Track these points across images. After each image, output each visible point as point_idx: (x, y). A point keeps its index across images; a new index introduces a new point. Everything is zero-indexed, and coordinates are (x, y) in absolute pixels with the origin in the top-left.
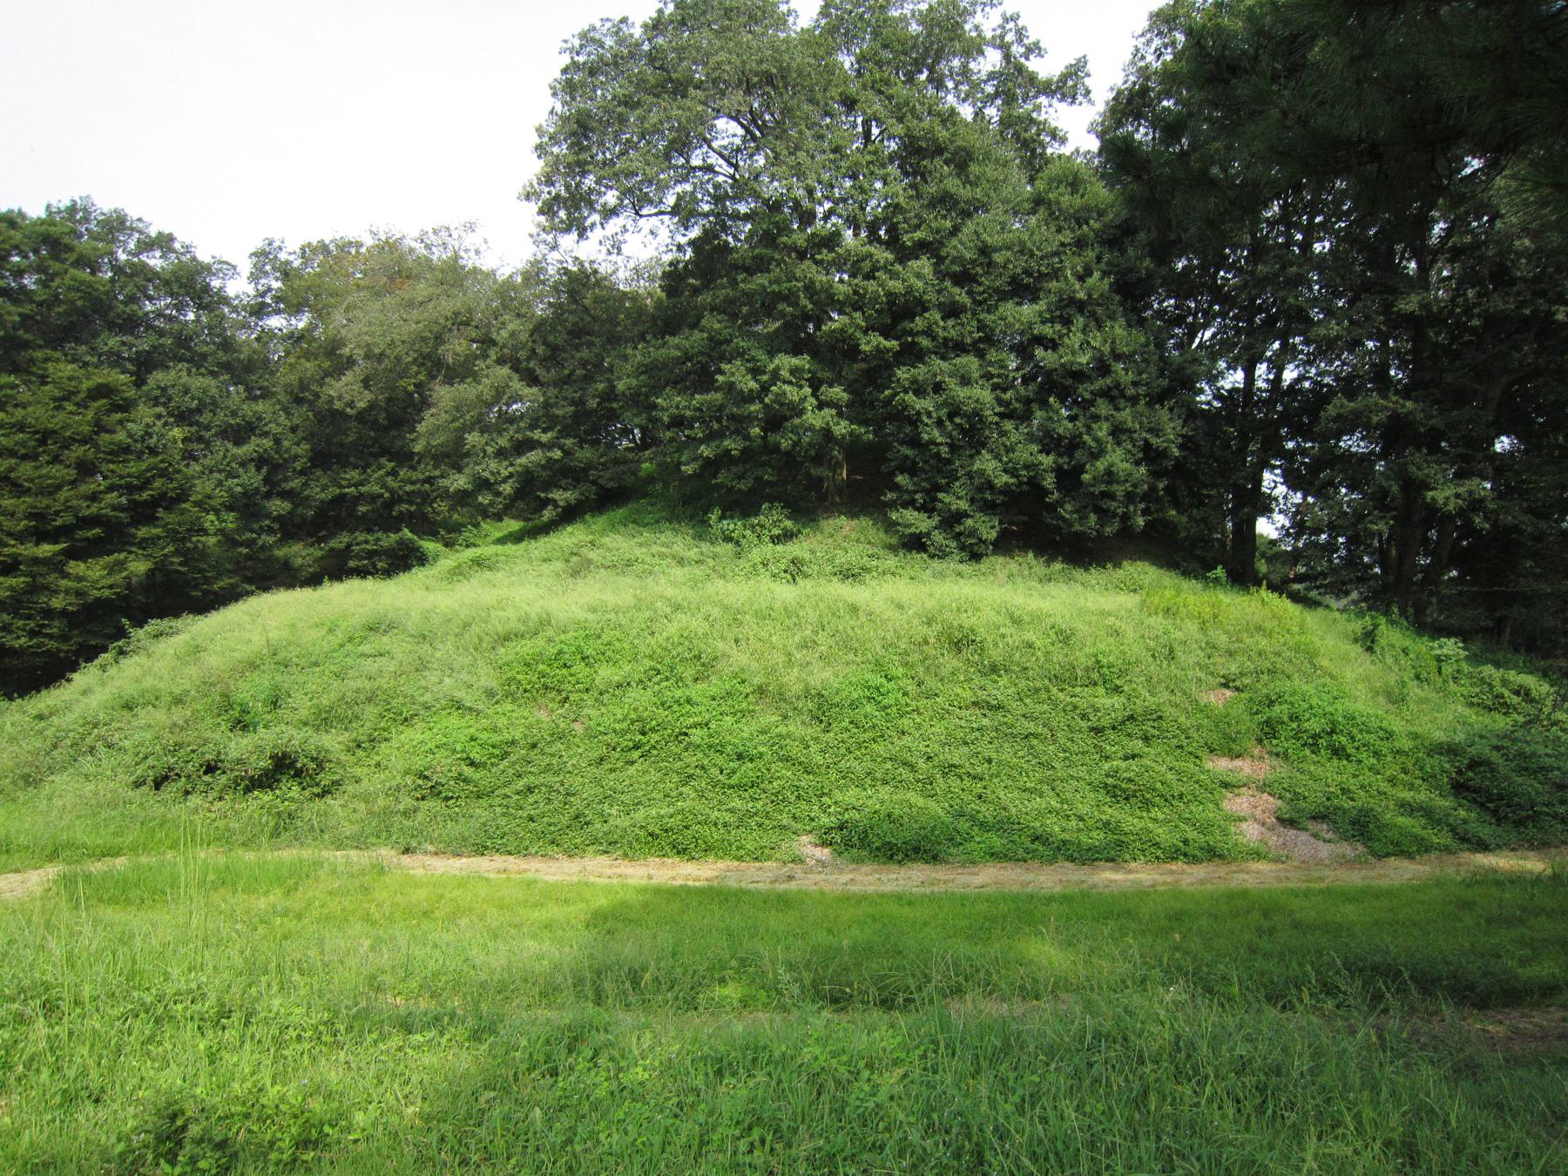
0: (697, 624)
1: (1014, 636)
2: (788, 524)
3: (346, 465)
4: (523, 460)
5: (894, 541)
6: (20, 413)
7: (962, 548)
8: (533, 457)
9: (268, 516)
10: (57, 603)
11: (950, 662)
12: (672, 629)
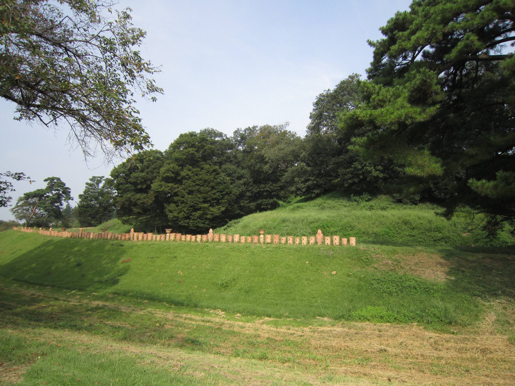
0: (350, 220)
1: (418, 221)
2: (370, 197)
3: (261, 183)
4: (307, 184)
5: (395, 200)
6: (200, 176)
7: (411, 202)
8: (310, 183)
9: (246, 196)
10: (208, 217)
11: (404, 227)
12: (345, 221)
